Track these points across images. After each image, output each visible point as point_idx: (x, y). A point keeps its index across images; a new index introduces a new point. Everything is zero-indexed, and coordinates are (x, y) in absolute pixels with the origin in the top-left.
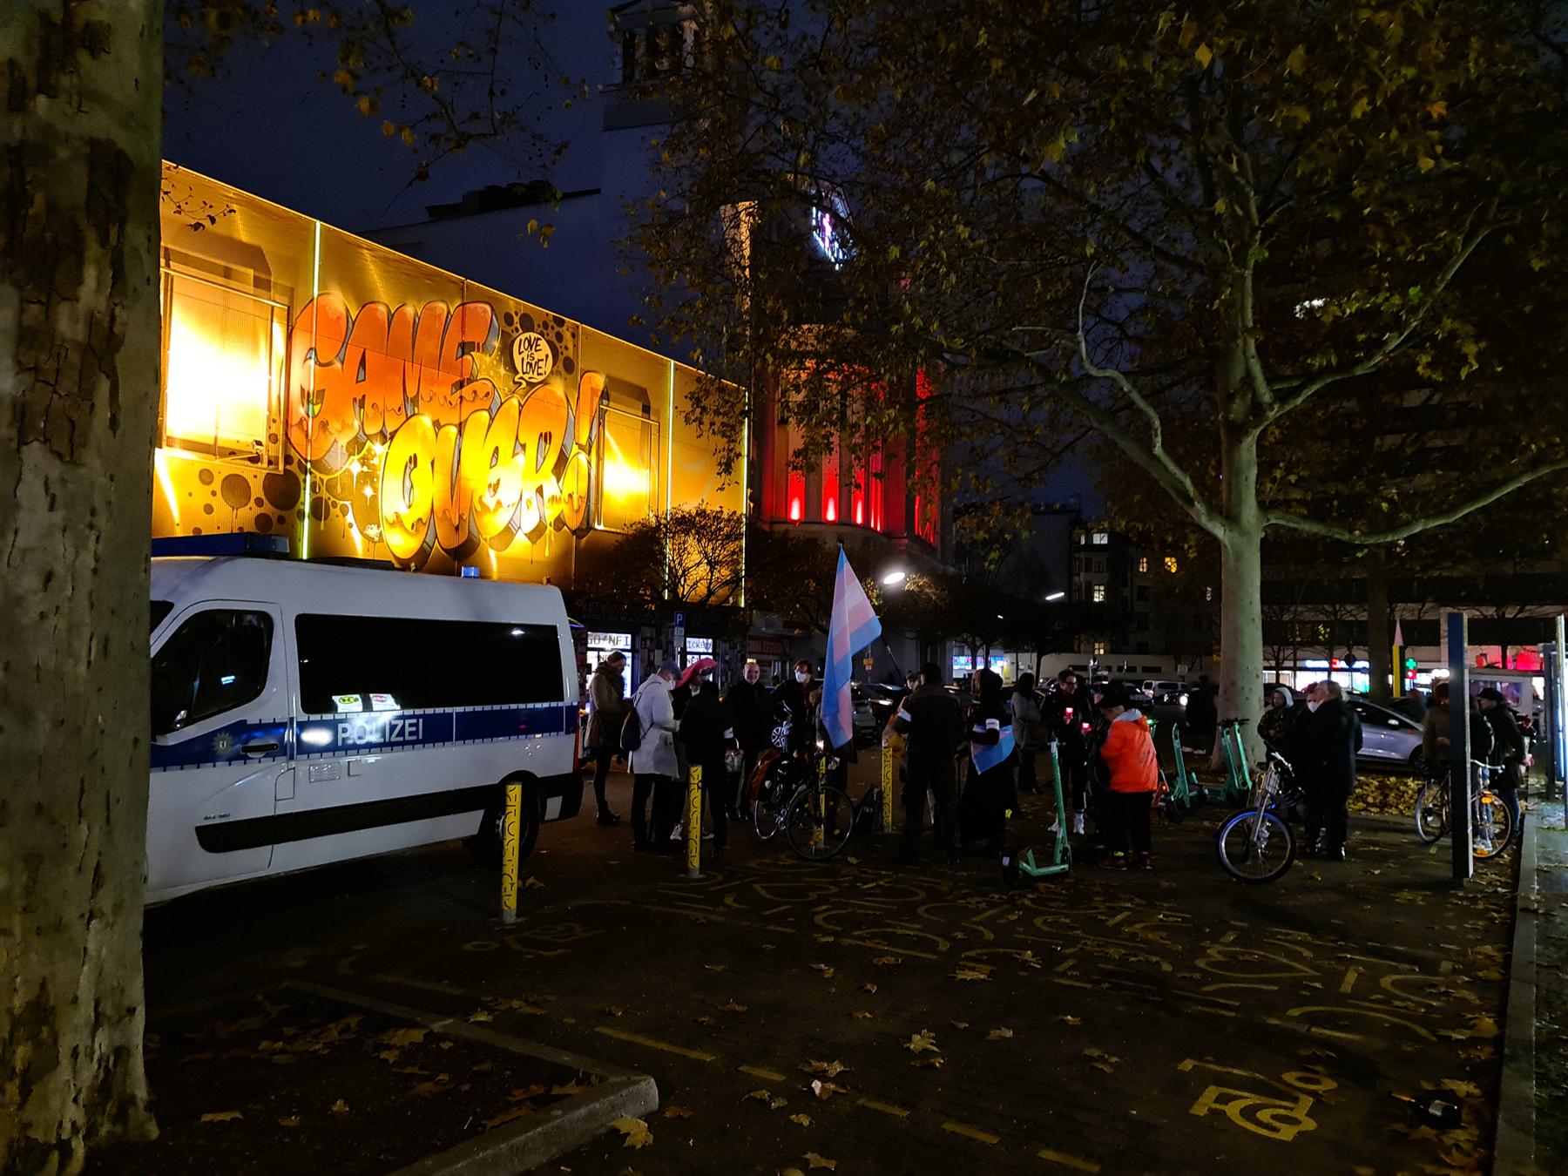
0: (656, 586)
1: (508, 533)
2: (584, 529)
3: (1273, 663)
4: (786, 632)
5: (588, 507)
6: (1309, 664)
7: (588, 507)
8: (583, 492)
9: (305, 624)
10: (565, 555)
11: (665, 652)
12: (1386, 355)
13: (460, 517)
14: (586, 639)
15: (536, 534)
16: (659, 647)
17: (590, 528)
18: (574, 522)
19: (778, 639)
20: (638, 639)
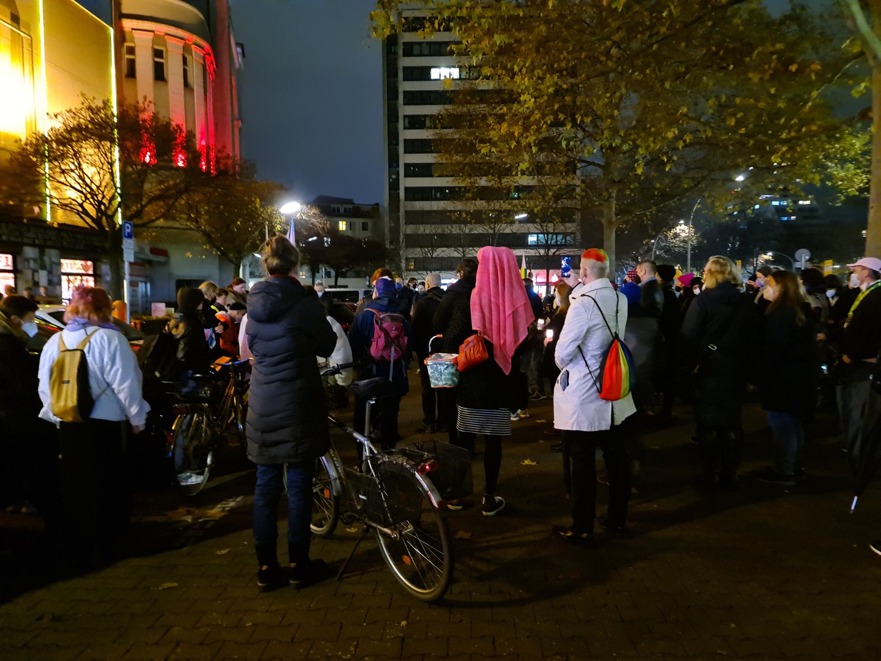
9: (526, 257)
11: (50, 273)
16: (43, 267)
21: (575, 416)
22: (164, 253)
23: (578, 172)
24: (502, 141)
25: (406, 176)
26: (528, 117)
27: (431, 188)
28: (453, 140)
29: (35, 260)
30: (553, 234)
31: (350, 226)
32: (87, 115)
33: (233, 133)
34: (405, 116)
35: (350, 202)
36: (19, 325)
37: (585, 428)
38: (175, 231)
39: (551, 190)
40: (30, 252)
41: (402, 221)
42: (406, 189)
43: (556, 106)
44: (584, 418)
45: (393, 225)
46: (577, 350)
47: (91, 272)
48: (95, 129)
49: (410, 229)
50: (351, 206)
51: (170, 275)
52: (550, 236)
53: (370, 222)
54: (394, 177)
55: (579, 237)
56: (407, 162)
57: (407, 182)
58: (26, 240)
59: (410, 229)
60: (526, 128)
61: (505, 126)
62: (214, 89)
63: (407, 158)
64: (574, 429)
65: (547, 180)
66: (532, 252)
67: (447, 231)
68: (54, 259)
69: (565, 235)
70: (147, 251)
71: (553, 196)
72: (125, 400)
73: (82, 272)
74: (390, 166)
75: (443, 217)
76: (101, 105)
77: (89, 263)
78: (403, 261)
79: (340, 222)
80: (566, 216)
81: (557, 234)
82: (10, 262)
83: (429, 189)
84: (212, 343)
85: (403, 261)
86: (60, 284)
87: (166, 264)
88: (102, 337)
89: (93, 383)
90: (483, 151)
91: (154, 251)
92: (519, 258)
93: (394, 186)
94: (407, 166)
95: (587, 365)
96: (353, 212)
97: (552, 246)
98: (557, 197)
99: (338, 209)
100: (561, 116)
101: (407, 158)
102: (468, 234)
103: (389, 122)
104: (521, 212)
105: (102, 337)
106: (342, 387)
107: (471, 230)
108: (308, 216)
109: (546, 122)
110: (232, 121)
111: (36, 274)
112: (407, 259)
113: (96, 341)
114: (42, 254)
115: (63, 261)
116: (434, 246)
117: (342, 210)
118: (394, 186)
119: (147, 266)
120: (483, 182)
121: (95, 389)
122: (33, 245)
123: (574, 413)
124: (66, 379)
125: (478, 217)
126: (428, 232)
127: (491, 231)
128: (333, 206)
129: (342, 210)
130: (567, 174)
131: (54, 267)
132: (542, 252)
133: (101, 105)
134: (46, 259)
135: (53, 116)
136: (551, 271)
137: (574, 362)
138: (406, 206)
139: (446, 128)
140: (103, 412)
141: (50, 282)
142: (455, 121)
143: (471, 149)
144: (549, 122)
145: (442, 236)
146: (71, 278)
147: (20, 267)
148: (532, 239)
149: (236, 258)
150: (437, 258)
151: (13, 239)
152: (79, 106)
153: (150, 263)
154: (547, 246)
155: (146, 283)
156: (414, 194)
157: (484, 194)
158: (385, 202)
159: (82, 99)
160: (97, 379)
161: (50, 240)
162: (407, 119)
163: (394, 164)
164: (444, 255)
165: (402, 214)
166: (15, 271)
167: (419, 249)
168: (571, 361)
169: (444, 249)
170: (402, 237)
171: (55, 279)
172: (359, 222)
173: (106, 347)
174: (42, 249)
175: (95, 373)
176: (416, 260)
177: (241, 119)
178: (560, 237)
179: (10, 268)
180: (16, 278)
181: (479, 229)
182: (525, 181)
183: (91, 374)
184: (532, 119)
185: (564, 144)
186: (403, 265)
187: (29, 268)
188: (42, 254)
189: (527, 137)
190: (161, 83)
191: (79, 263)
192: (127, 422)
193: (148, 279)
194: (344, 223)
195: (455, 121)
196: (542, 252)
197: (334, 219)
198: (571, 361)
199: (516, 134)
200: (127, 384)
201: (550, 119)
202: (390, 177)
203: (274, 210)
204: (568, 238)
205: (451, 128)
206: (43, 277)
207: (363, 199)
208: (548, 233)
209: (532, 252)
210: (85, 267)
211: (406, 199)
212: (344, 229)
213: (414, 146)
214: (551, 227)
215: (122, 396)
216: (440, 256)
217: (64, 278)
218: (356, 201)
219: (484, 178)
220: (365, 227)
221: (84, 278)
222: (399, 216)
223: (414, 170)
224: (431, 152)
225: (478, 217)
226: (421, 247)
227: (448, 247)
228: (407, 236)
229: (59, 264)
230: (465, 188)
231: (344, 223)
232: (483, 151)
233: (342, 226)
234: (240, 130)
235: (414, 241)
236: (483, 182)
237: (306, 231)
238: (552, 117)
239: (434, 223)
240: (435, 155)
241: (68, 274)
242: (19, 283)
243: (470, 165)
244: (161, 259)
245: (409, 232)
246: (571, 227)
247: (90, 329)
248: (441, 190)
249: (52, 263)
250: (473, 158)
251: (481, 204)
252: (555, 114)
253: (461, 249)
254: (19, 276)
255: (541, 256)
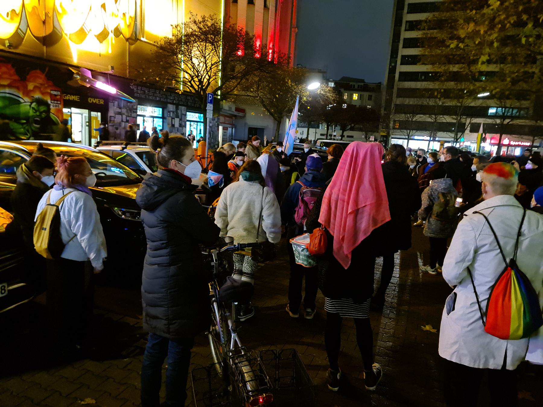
0: (327, 101)
1: (82, 33)
2: (134, 39)
3: (407, 137)
4: (236, 113)
5: (135, 24)
6: (416, 137)
7: (135, 24)
8: (133, 15)
9: (484, 124)
10: (122, 55)
11: (181, 120)
12: (536, 122)
13: (46, 14)
14: (136, 109)
15: (102, 36)
16: (177, 117)
17: (137, 39)
18: (127, 32)
19: (232, 116)
20: (165, 112)
21: (455, 347)
22: (243, 111)
23: (538, 63)
24: (469, 38)
25: (401, 64)
26: (494, 18)
27: (418, 73)
28: (435, 38)
29: (173, 112)
30: (510, 108)
31: (360, 97)
32: (195, 28)
33: (290, 37)
34: (407, 22)
35: (362, 81)
36: (39, 178)
37: (467, 362)
38: (245, 97)
39: (510, 77)
40: (171, 107)
41: (395, 95)
42: (400, 73)
43: (521, 8)
44: (465, 352)
45: (388, 97)
46: (466, 273)
47: (202, 120)
48: (207, 34)
49: (399, 101)
50: (362, 84)
51: (246, 124)
52: (507, 109)
53: (373, 95)
54: (393, 65)
55: (531, 112)
56: (404, 54)
57: (402, 68)
58: (169, 101)
59: (399, 101)
60: (492, 27)
61: (472, 25)
62: (281, 8)
63: (404, 52)
64: (454, 360)
65: (508, 68)
66: (490, 121)
67: (425, 103)
68: (184, 112)
69: (520, 109)
70: (234, 109)
71: (510, 82)
72: (86, 248)
73: (198, 120)
74: (392, 57)
75: (430, 93)
76: (201, 20)
77: (202, 115)
78: (392, 123)
79: (354, 94)
80: (521, 96)
81: (513, 109)
82: (161, 113)
83: (417, 73)
84: (221, 184)
85: (392, 123)
86: (185, 127)
87: (244, 117)
88: (72, 198)
89: (63, 232)
90: (452, 46)
91: (237, 109)
92: (479, 125)
93: (392, 70)
94: (403, 57)
95: (475, 292)
96: (363, 87)
97: (508, 117)
98: (514, 82)
99: (354, 85)
100: (525, 17)
101: (404, 52)
102: (440, 106)
103: (395, 26)
104: (484, 91)
105: (72, 198)
106: (273, 243)
107: (443, 103)
108: (326, 92)
109: (509, 22)
110: (291, 29)
111: (173, 120)
112: (395, 121)
113: (67, 201)
114: (177, 109)
115: (188, 113)
116: (414, 113)
117: (356, 87)
118: (392, 70)
119: (234, 118)
120: (455, 68)
121: (65, 237)
122: (172, 103)
123: (455, 343)
124: (44, 227)
125: (447, 94)
126: (411, 103)
127: (459, 104)
128: (351, 83)
129: (356, 87)
130: (526, 64)
131: (183, 116)
132: (498, 121)
133: (201, 20)
134: (179, 112)
135: (174, 26)
136: (503, 136)
137: (463, 284)
138: (399, 84)
139: (431, 29)
140: (70, 254)
141: (180, 125)
142: (439, 25)
143: (442, 43)
144: (512, 22)
145: (422, 106)
146: (192, 123)
147: (165, 115)
148: (492, 111)
149: (279, 117)
150: (416, 122)
151: (162, 100)
152: (188, 20)
153: (235, 116)
154: (503, 117)
155: (232, 129)
156: (405, 76)
157: (455, 77)
158: (385, 81)
159: (190, 16)
160: (66, 229)
161: (181, 101)
162: (408, 24)
163: (395, 56)
164: (420, 120)
165: (395, 90)
166: (163, 118)
167: (403, 115)
168: (460, 283)
169: (422, 116)
170: (393, 106)
171: (183, 124)
172: (366, 94)
173: (73, 205)
174: (177, 106)
175: (64, 224)
176: (401, 122)
177: (297, 27)
178: (515, 111)
179: (161, 116)
180: (163, 122)
181: (449, 103)
182: (484, 68)
183: (62, 225)
184: (497, 20)
185: (523, 40)
186: (391, 125)
187: (170, 117)
188: (177, 109)
189: (490, 35)
190: (251, 6)
191: (197, 115)
192: (89, 262)
193: (233, 126)
194: (357, 95)
195: (439, 25)
196: (498, 121)
197: (352, 92)
198: (460, 283)
199: (482, 32)
200: (86, 236)
201: (513, 19)
202: (390, 65)
203: (303, 87)
204: (522, 112)
205: (435, 29)
206: (177, 122)
207: (370, 80)
208: (506, 108)
209: (490, 121)
210: (200, 117)
211: (400, 80)
212: (356, 98)
213: (410, 43)
214: (508, 103)
215: (83, 245)
216: (419, 120)
217: (188, 123)
218: (366, 81)
219: (457, 66)
220: (370, 98)
221: (199, 124)
222: (393, 91)
223: (407, 60)
224: (418, 47)
225: (447, 94)
226: (405, 113)
227: (424, 114)
228: (396, 105)
229: (186, 115)
230: (441, 73)
231: (357, 95)
232: (452, 46)
233: (355, 97)
234: (296, 34)
235: (400, 109)
236: (455, 68)
237: (323, 101)
238: (515, 18)
239: (416, 98)
240: (420, 49)
241: (191, 121)
242: (165, 124)
243: (446, 56)
244: (241, 114)
245: (398, 103)
246: (525, 103)
247: (67, 191)
248: (426, 74)
249: (182, 114)
250: (446, 51)
251: (451, 85)
252: (519, 15)
253: (433, 116)
254: (165, 120)
255: (496, 124)
